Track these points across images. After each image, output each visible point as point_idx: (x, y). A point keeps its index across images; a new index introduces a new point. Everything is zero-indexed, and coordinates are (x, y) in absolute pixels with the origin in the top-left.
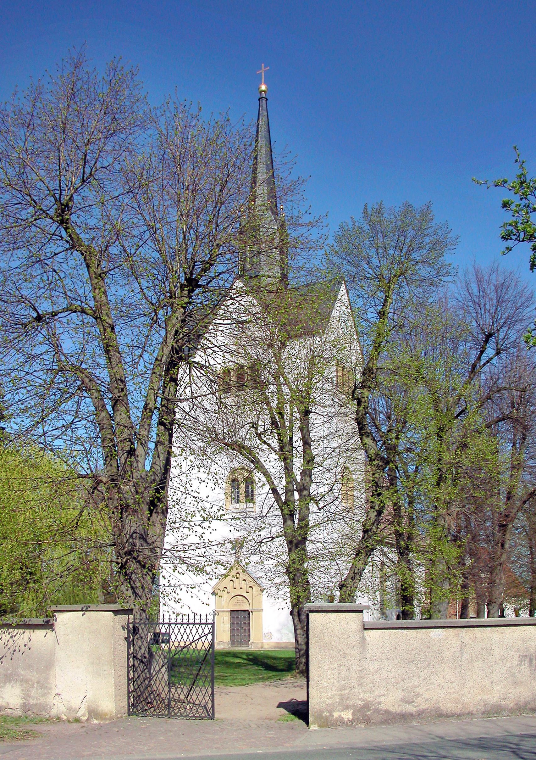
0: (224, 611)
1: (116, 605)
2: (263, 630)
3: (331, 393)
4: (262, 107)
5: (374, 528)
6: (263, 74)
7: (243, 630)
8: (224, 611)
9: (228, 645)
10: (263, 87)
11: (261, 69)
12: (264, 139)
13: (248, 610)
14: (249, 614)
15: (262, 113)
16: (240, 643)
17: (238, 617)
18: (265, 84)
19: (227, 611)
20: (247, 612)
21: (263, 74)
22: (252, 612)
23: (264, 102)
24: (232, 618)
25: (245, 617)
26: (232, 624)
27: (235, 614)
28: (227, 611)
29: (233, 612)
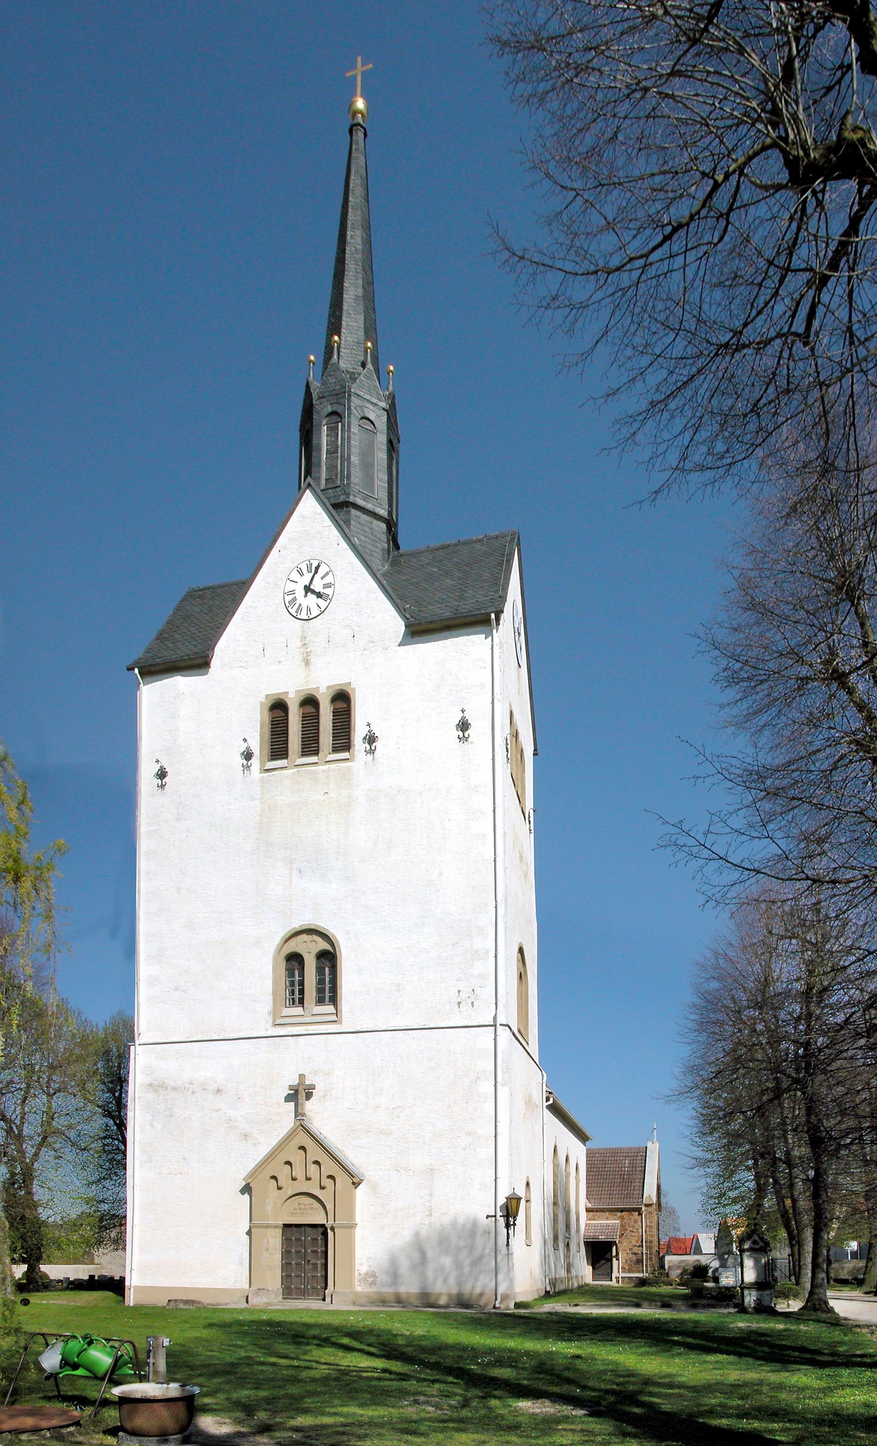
0: (267, 1227)
1: (670, 1287)
2: (357, 1267)
3: (834, 934)
4: (357, 144)
5: (829, 1099)
6: (359, 78)
7: (311, 1267)
8: (267, 1227)
9: (277, 1295)
10: (360, 104)
11: (355, 67)
12: (359, 213)
13: (323, 1226)
14: (325, 1234)
15: (357, 158)
16: (303, 1294)
17: (298, 1240)
18: (362, 96)
19: (276, 1227)
20: (320, 1230)
21: (359, 78)
22: (333, 1229)
23: (361, 134)
24: (287, 1242)
25: (314, 1240)
26: (286, 1254)
27: (294, 1234)
28: (276, 1227)
29: (289, 1229)
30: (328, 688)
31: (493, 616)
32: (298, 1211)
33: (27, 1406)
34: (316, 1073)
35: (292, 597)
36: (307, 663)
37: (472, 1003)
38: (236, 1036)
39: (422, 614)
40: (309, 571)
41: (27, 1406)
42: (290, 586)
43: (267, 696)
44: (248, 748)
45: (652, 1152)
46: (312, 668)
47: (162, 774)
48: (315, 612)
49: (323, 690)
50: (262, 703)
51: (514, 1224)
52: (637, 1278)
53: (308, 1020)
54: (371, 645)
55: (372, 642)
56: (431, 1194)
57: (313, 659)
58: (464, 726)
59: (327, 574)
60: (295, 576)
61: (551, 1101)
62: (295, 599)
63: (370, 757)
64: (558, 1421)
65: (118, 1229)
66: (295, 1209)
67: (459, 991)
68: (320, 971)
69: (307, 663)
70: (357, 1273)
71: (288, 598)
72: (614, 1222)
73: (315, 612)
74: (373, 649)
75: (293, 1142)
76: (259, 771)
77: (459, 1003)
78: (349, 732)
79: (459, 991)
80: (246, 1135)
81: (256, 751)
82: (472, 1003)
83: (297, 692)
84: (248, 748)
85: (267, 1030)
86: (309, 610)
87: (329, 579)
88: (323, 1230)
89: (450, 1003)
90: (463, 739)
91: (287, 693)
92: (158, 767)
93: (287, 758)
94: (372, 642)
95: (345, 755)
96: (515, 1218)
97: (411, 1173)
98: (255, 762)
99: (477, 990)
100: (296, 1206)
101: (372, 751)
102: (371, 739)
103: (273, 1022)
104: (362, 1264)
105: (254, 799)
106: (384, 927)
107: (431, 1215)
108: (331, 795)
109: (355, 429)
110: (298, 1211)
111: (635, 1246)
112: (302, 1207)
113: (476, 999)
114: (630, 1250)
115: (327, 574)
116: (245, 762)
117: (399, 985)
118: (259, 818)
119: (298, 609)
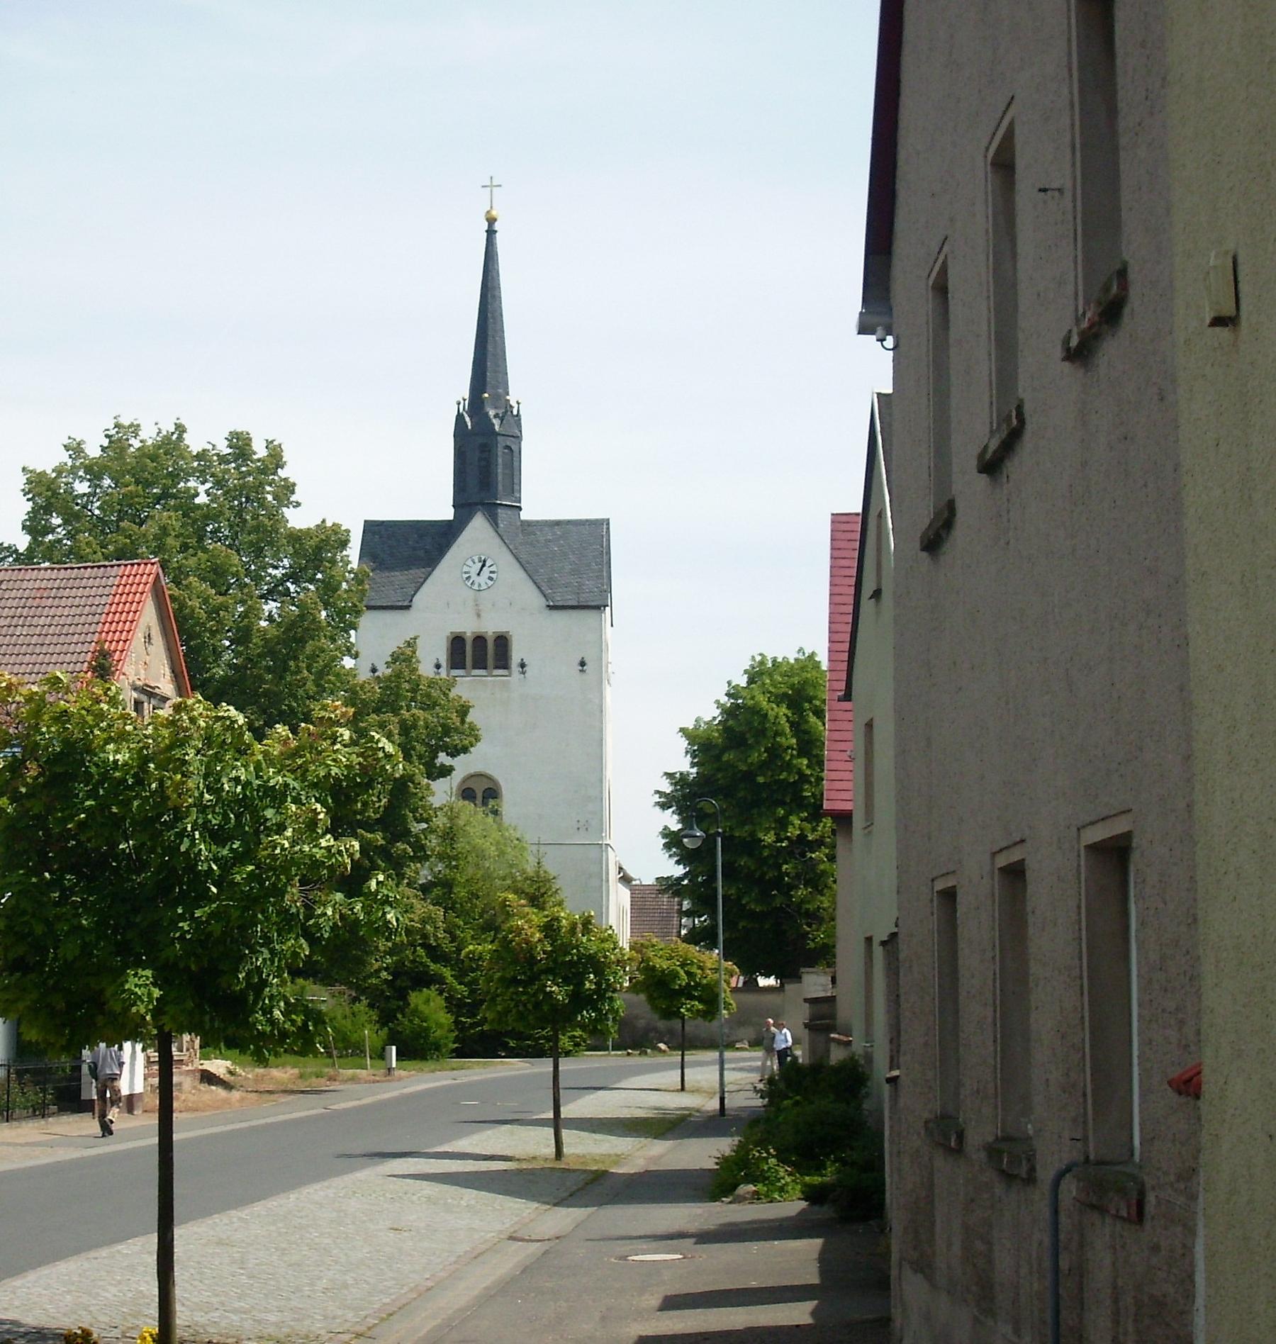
33: (935, 899)
35: (468, 575)
36: (479, 616)
40: (480, 561)
41: (935, 899)
42: (466, 569)
43: (451, 633)
45: (474, 1165)
49: (490, 633)
50: (448, 637)
52: (397, 1060)
57: (483, 614)
59: (492, 565)
60: (469, 563)
61: (622, 874)
64: (603, 1140)
69: (479, 616)
73: (484, 587)
77: (578, 829)
81: (444, 663)
86: (480, 585)
91: (465, 633)
101: (524, 673)
102: (523, 665)
115: (492, 565)
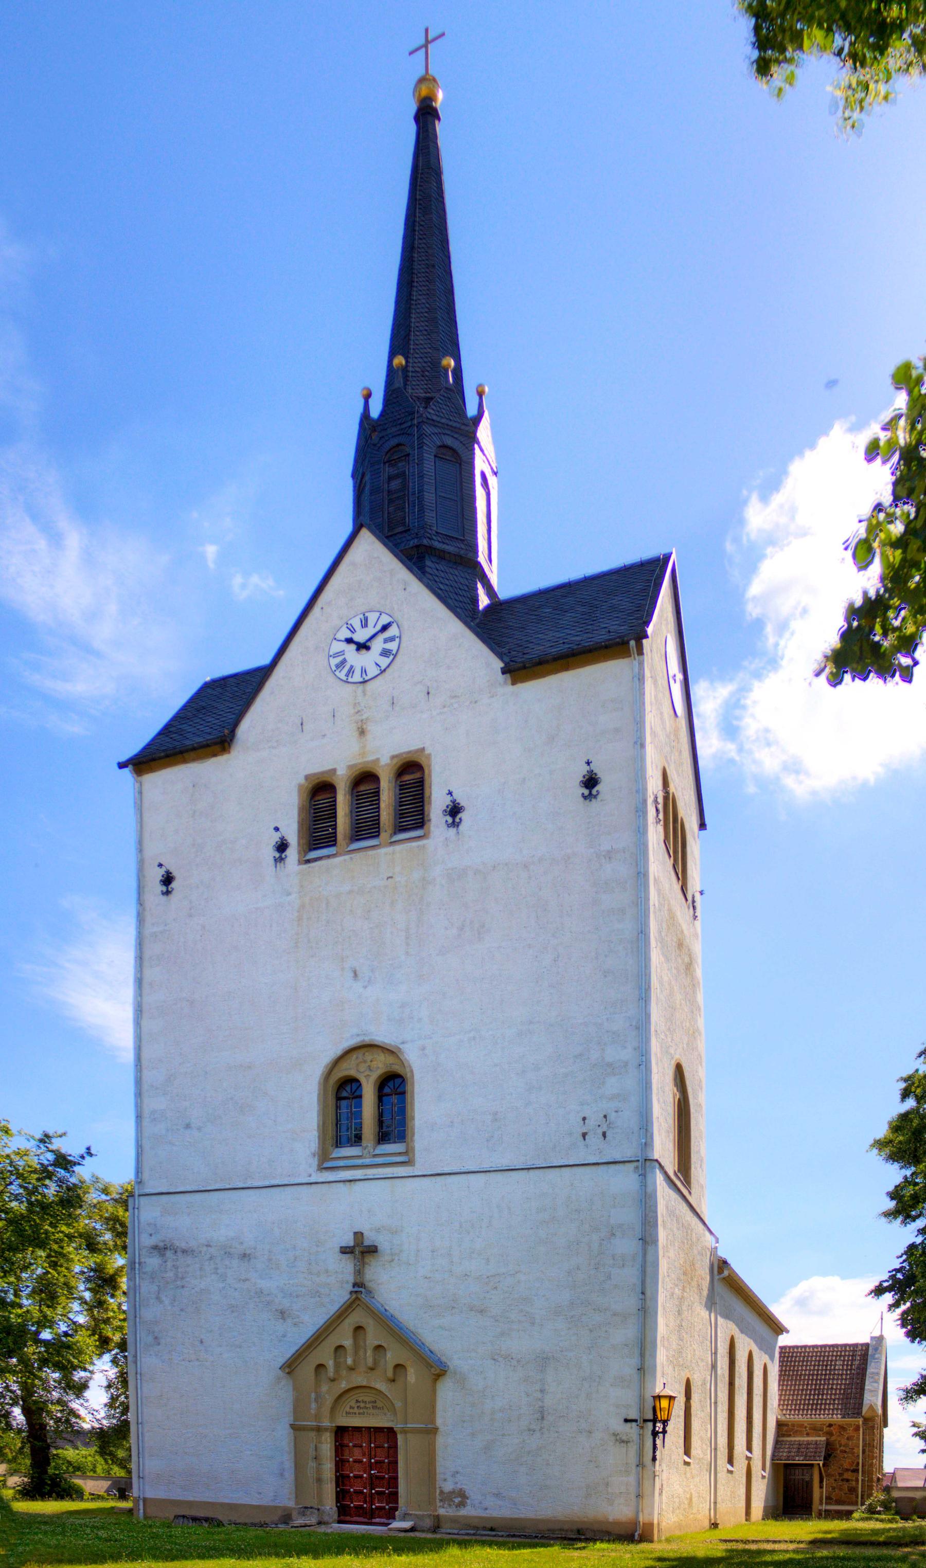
30: (393, 757)
31: (632, 643)
32: (356, 1410)
34: (378, 1230)
36: (362, 732)
37: (604, 1135)
38: (267, 1183)
39: (527, 656)
44: (282, 839)
46: (369, 737)
47: (168, 880)
48: (372, 671)
49: (385, 760)
51: (664, 1432)
53: (367, 1161)
54: (453, 701)
55: (455, 697)
56: (542, 1391)
58: (591, 782)
62: (344, 662)
63: (453, 831)
65: (12, 1157)
66: (351, 1407)
67: (584, 1119)
68: (381, 1096)
69: (362, 732)
70: (438, 1491)
71: (334, 662)
72: (818, 1439)
74: (456, 706)
75: (347, 1321)
76: (297, 862)
77: (584, 1135)
78: (423, 806)
79: (584, 1119)
80: (282, 1313)
81: (293, 839)
82: (604, 1135)
83: (350, 767)
84: (282, 839)
85: (310, 1176)
86: (364, 671)
87: (393, 646)
88: (391, 1433)
89: (571, 1134)
90: (589, 797)
91: (334, 770)
92: (162, 871)
93: (334, 845)
94: (455, 697)
95: (419, 833)
96: (665, 1422)
97: (514, 1363)
98: (292, 853)
99: (612, 1116)
100: (353, 1403)
102: (454, 811)
103: (319, 1165)
104: (445, 1480)
105: (289, 894)
106: (474, 1038)
107: (543, 1418)
108: (398, 879)
109: (429, 464)
110: (356, 1410)
111: (847, 1470)
112: (362, 1405)
113: (609, 1127)
114: (840, 1474)
116: (277, 855)
117: (496, 1113)
118: (296, 914)
119: (349, 671)
